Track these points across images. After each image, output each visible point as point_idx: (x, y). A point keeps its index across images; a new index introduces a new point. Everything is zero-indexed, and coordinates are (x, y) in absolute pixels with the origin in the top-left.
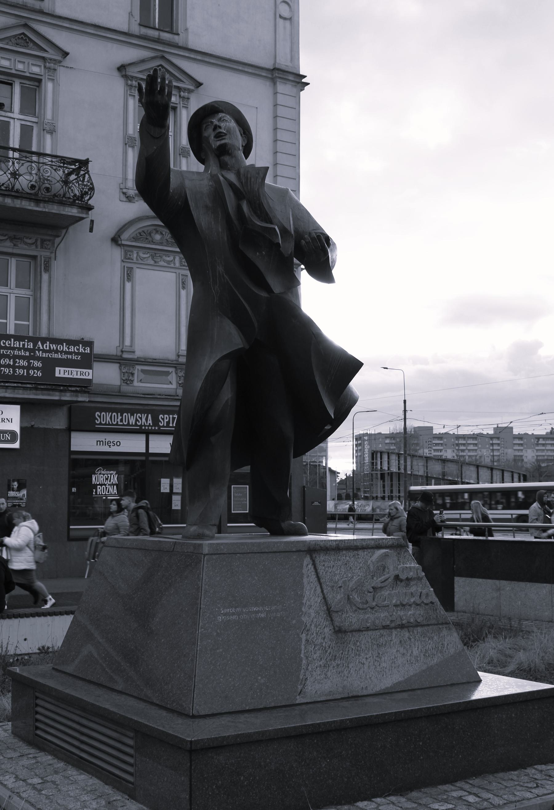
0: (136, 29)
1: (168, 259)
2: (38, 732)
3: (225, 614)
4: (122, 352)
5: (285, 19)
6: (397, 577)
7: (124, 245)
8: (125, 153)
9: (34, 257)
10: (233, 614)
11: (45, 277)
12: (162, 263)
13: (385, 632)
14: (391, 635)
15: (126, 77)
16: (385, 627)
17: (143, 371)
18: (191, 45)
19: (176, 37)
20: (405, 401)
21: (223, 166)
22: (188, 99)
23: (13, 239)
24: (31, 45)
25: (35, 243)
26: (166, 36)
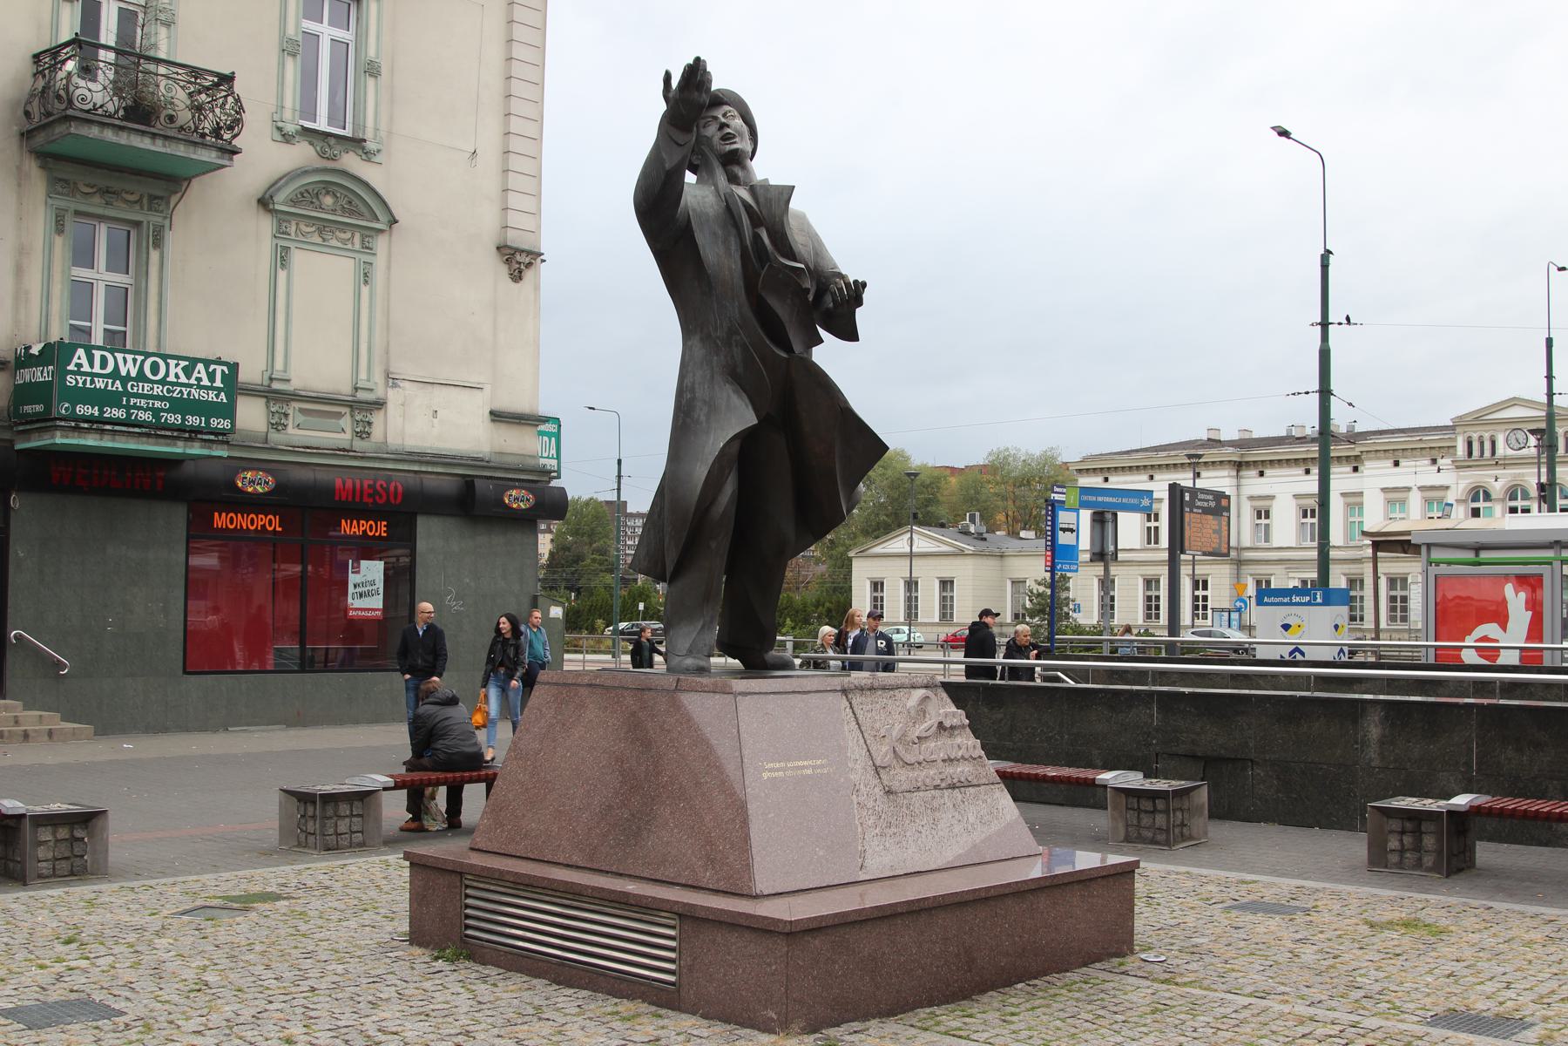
1: (343, 236)
2: (469, 932)
3: (770, 770)
4: (271, 379)
7: (277, 211)
8: (282, 65)
9: (137, 224)
10: (778, 770)
11: (154, 255)
12: (334, 243)
13: (937, 793)
16: (936, 787)
17: (302, 411)
20: (619, 462)
21: (733, 179)
23: (105, 192)
25: (139, 201)
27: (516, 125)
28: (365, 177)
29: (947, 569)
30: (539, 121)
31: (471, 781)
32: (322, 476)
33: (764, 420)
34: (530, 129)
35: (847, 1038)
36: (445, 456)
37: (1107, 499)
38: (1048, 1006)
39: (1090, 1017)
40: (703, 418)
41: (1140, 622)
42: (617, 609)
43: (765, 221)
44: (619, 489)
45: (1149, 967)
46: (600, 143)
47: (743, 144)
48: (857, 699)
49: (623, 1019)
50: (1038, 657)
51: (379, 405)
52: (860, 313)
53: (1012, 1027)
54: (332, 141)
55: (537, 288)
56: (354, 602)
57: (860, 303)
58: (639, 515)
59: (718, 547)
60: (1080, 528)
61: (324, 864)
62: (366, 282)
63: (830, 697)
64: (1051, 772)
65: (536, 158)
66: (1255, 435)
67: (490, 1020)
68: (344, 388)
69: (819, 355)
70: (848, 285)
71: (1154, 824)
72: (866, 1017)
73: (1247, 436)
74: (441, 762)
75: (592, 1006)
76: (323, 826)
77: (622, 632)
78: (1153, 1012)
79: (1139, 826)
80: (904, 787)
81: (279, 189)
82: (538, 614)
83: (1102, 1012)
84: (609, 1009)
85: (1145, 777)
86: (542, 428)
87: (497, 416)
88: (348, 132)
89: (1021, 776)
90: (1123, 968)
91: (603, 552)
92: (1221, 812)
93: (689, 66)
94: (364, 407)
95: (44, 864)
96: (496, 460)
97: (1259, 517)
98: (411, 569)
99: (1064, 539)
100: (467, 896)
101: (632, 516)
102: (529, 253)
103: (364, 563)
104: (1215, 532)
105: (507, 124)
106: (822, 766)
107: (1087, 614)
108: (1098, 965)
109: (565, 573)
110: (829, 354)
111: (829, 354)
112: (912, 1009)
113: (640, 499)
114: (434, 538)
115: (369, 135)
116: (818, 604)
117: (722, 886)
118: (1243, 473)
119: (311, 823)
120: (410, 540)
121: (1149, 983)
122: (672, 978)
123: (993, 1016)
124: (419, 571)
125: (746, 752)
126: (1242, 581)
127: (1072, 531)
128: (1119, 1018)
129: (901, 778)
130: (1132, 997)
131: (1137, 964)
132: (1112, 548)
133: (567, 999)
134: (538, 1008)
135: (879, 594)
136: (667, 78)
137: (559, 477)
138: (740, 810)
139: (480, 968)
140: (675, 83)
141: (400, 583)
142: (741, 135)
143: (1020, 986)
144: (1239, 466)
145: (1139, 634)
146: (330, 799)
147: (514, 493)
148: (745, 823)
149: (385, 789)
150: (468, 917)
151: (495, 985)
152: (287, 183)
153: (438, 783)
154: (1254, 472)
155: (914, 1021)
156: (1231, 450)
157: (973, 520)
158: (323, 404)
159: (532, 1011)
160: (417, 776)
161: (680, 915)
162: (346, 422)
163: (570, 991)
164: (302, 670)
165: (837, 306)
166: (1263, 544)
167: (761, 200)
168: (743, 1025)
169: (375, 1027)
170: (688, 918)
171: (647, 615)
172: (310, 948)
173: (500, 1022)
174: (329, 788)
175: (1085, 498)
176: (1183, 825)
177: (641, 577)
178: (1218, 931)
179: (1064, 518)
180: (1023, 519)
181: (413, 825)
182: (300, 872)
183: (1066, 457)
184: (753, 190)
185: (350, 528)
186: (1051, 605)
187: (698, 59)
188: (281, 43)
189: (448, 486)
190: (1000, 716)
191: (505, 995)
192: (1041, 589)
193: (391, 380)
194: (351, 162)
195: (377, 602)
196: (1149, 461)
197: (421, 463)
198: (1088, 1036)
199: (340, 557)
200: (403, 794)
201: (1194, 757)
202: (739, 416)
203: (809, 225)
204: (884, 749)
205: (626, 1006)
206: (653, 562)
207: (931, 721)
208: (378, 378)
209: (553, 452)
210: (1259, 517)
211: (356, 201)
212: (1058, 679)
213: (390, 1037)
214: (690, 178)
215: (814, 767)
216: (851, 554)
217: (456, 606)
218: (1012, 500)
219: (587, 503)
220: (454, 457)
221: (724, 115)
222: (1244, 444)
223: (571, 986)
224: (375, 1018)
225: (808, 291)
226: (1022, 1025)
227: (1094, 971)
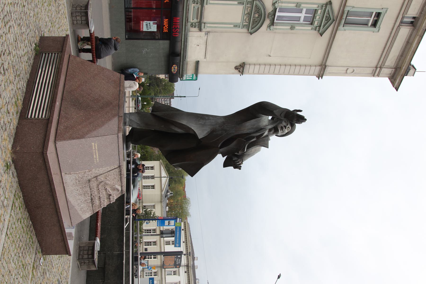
0: (347, 9)
1: (247, 20)
2: (44, 55)
3: (95, 145)
5: (347, 71)
6: (111, 195)
8: (293, 3)
10: (95, 147)
11: (236, 3)
12: (245, 17)
13: (90, 195)
14: (88, 196)
15: (326, 4)
16: (91, 195)
17: (198, 8)
18: (338, 32)
19: (342, 26)
20: (185, 97)
21: (270, 130)
22: (316, 30)
24: (326, 22)
26: (343, 21)
27: (278, 67)
28: (264, 23)
29: (157, 187)
30: (279, 74)
31: (93, 55)
32: (180, 14)
33: (200, 141)
34: (256, 70)
35: (11, 172)
36: (186, 48)
37: (178, 234)
38: (24, 232)
39: (21, 246)
40: (200, 122)
41: (144, 241)
42: (144, 97)
43: (258, 140)
44: (177, 97)
45: (38, 261)
46: (283, 92)
47: (280, 133)
48: (117, 170)
49: (16, 102)
50: (133, 216)
51: (200, 30)
52: (232, 168)
53: (16, 223)
54: (273, 17)
55: (233, 74)
56: (145, 23)
57: (235, 168)
58: (170, 103)
59: (162, 128)
60: (170, 226)
61: (66, 12)
62: (234, 26)
63: (118, 162)
64: (99, 224)
65: (269, 73)
66: (196, 270)
67: (14, 61)
68: (205, 20)
69: (219, 156)
70: (240, 164)
71: (85, 254)
72: (18, 176)
73: (196, 268)
74: (98, 46)
75: (20, 92)
76: (78, 12)
77: (138, 98)
78: (23, 265)
79: (84, 250)
80: (91, 185)
81: (260, 2)
82: (142, 75)
83: (22, 249)
84: (19, 98)
85: (98, 251)
86: (194, 75)
87: (197, 63)
88: (275, 21)
89: (97, 217)
90: (38, 253)
91: (160, 92)
92: (89, 274)
93: (304, 117)
94: (200, 26)
95: (168, 102)
96: (185, 63)
97: (174, 272)
98: (154, 39)
99: (166, 222)
100: (55, 54)
101: (170, 100)
102: (243, 71)
103: (156, 25)
104: (170, 264)
105: (278, 65)
106: (96, 161)
107: (146, 226)
108: (38, 245)
109: (154, 82)
110: (220, 159)
111: (220, 159)
112: (22, 191)
113: (175, 104)
114: (163, 45)
115: (275, 27)
116: (147, 152)
117: (59, 131)
118: (186, 267)
119: (79, 8)
120: (162, 39)
121: (33, 261)
122: (29, 117)
123: (20, 216)
124: (154, 41)
125: (100, 138)
126: (156, 268)
127: (169, 224)
128: (21, 255)
129: (94, 184)
130: (28, 258)
131: (39, 257)
132: (164, 236)
133: (23, 84)
134: (19, 75)
135: (150, 168)
136: (300, 111)
137: (181, 80)
138: (82, 137)
139: (33, 58)
140: (299, 113)
141: (151, 36)
142: (283, 132)
143: (31, 223)
144: (187, 266)
145: (140, 241)
146: (86, 14)
147: (176, 68)
148: (78, 138)
149: (90, 30)
150: (49, 54)
151: (27, 62)
152: (261, 4)
153: (92, 46)
154: (186, 270)
155: (17, 192)
156: (192, 263)
157: (171, 194)
158: (200, 14)
159: (18, 73)
160: (94, 40)
161: (49, 119)
162: (195, 20)
163: (25, 85)
164: (125, 8)
165: (234, 161)
166: (166, 273)
167: (264, 139)
168: (14, 139)
169: (11, 25)
170: (48, 122)
171: (143, 105)
172: (38, 6)
173: (14, 64)
174: (90, 14)
175: (178, 228)
176: (84, 263)
177: (153, 103)
178: (51, 279)
179: (172, 222)
180: (171, 207)
181: (80, 39)
182: (64, 4)
183: (189, 218)
184: (267, 136)
185: (166, 21)
186: (148, 217)
187: (306, 120)
188: (300, 3)
189: (178, 49)
190: (115, 207)
191: (23, 66)
192: (152, 213)
193: (207, 33)
194: (267, 22)
195: (145, 29)
196: (189, 243)
197: (184, 42)
198: (14, 246)
199: (158, 19)
200: (89, 36)
201: (105, 264)
202: (201, 133)
203: (257, 152)
204: (102, 179)
205: (20, 103)
206: (157, 108)
207: (111, 192)
208: (208, 29)
209: (188, 79)
210: (174, 272)
211: (257, 23)
212: (126, 222)
213: (8, 29)
214: (270, 118)
215: (96, 158)
216: (161, 161)
217: (144, 52)
218: (177, 207)
219: (173, 88)
220: (186, 51)
221: (288, 127)
222: (194, 267)
223: (27, 86)
224: (14, 25)
225: (238, 153)
226: (17, 225)
227: (36, 244)
